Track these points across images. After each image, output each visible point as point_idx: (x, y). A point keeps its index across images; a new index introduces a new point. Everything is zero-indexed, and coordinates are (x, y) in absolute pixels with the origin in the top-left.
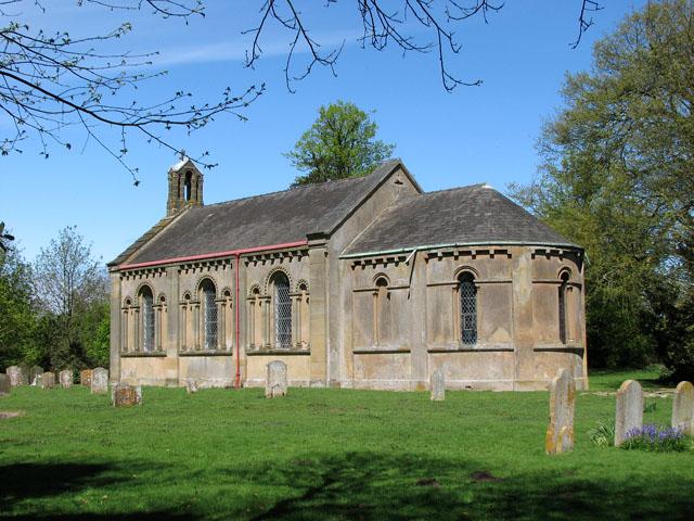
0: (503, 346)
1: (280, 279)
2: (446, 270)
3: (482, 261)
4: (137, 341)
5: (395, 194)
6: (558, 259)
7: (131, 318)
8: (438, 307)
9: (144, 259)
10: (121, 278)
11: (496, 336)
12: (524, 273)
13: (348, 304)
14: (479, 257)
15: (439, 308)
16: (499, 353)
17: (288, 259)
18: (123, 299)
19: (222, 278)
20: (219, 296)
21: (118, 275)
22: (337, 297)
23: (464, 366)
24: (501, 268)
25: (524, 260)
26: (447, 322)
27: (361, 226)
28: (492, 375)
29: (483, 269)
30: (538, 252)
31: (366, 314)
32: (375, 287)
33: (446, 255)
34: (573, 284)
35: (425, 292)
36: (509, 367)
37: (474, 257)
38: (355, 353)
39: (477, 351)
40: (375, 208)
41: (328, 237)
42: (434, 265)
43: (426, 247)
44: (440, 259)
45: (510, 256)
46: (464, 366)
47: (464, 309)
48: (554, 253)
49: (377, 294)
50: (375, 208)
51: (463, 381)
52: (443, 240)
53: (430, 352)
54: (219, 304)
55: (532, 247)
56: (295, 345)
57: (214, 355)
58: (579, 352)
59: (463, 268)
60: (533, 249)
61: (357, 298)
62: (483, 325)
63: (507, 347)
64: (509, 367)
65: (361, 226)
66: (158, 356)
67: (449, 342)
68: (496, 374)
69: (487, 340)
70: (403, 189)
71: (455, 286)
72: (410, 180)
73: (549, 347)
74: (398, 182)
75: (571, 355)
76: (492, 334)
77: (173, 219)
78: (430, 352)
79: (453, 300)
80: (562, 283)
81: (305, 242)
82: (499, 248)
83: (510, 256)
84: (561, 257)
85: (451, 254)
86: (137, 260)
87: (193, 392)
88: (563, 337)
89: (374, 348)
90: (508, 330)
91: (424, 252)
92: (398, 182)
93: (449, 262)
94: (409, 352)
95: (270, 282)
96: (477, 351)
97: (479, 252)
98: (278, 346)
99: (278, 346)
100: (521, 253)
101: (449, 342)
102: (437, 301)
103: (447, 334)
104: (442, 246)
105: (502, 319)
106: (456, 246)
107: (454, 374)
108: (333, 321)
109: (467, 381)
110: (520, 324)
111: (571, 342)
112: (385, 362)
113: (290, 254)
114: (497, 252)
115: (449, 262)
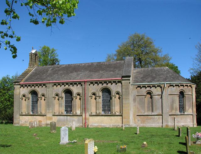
1: (34, 93)
4: (28, 110)
7: (93, 100)
8: (172, 101)
10: (20, 87)
13: (134, 100)
14: (185, 87)
15: (173, 102)
16: (190, 116)
17: (26, 87)
18: (21, 95)
19: (75, 90)
20: (75, 95)
21: (19, 86)
23: (181, 119)
26: (176, 106)
28: (188, 122)
31: (142, 103)
32: (145, 94)
33: (176, 85)
42: (171, 88)
43: (169, 83)
44: (174, 87)
46: (181, 119)
49: (22, 99)
52: (175, 81)
53: (170, 115)
54: (40, 99)
56: (40, 113)
57: (72, 116)
59: (180, 90)
61: (138, 99)
66: (41, 116)
67: (177, 112)
68: (189, 122)
71: (179, 95)
77: (33, 69)
78: (170, 115)
79: (177, 99)
81: (121, 78)
85: (178, 85)
86: (26, 80)
89: (146, 114)
91: (168, 84)
93: (177, 88)
95: (30, 94)
98: (31, 113)
99: (31, 113)
101: (177, 112)
102: (173, 99)
103: (176, 110)
104: (174, 83)
106: (180, 83)
107: (178, 122)
112: (150, 119)
113: (24, 86)
115: (177, 88)
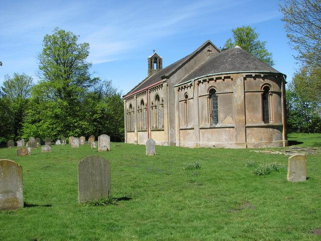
0: (229, 125)
2: (204, 89)
3: (219, 83)
5: (207, 56)
6: (261, 80)
9: (140, 90)
11: (226, 120)
12: (239, 87)
14: (218, 81)
16: (228, 129)
22: (174, 104)
24: (228, 86)
25: (239, 81)
27: (187, 71)
29: (219, 86)
30: (247, 76)
34: (271, 92)
35: (198, 100)
36: (232, 136)
37: (215, 81)
38: (201, 129)
39: (217, 128)
40: (195, 63)
41: (168, 77)
45: (232, 79)
47: (214, 107)
48: (259, 77)
50: (195, 63)
51: (211, 144)
55: (244, 74)
58: (279, 128)
59: (211, 87)
60: (244, 75)
62: (221, 115)
63: (231, 126)
64: (232, 136)
65: (187, 71)
69: (222, 123)
70: (212, 54)
71: (208, 96)
72: (215, 48)
73: (255, 125)
74: (209, 51)
75: (271, 129)
76: (226, 120)
79: (205, 101)
80: (264, 92)
82: (226, 75)
83: (232, 79)
84: (263, 78)
87: (93, 148)
88: (265, 118)
90: (232, 117)
92: (209, 51)
94: (194, 129)
96: (217, 128)
97: (217, 79)
100: (237, 77)
105: (229, 112)
106: (207, 76)
108: (171, 115)
109: (213, 143)
110: (238, 115)
111: (271, 123)
114: (225, 78)
